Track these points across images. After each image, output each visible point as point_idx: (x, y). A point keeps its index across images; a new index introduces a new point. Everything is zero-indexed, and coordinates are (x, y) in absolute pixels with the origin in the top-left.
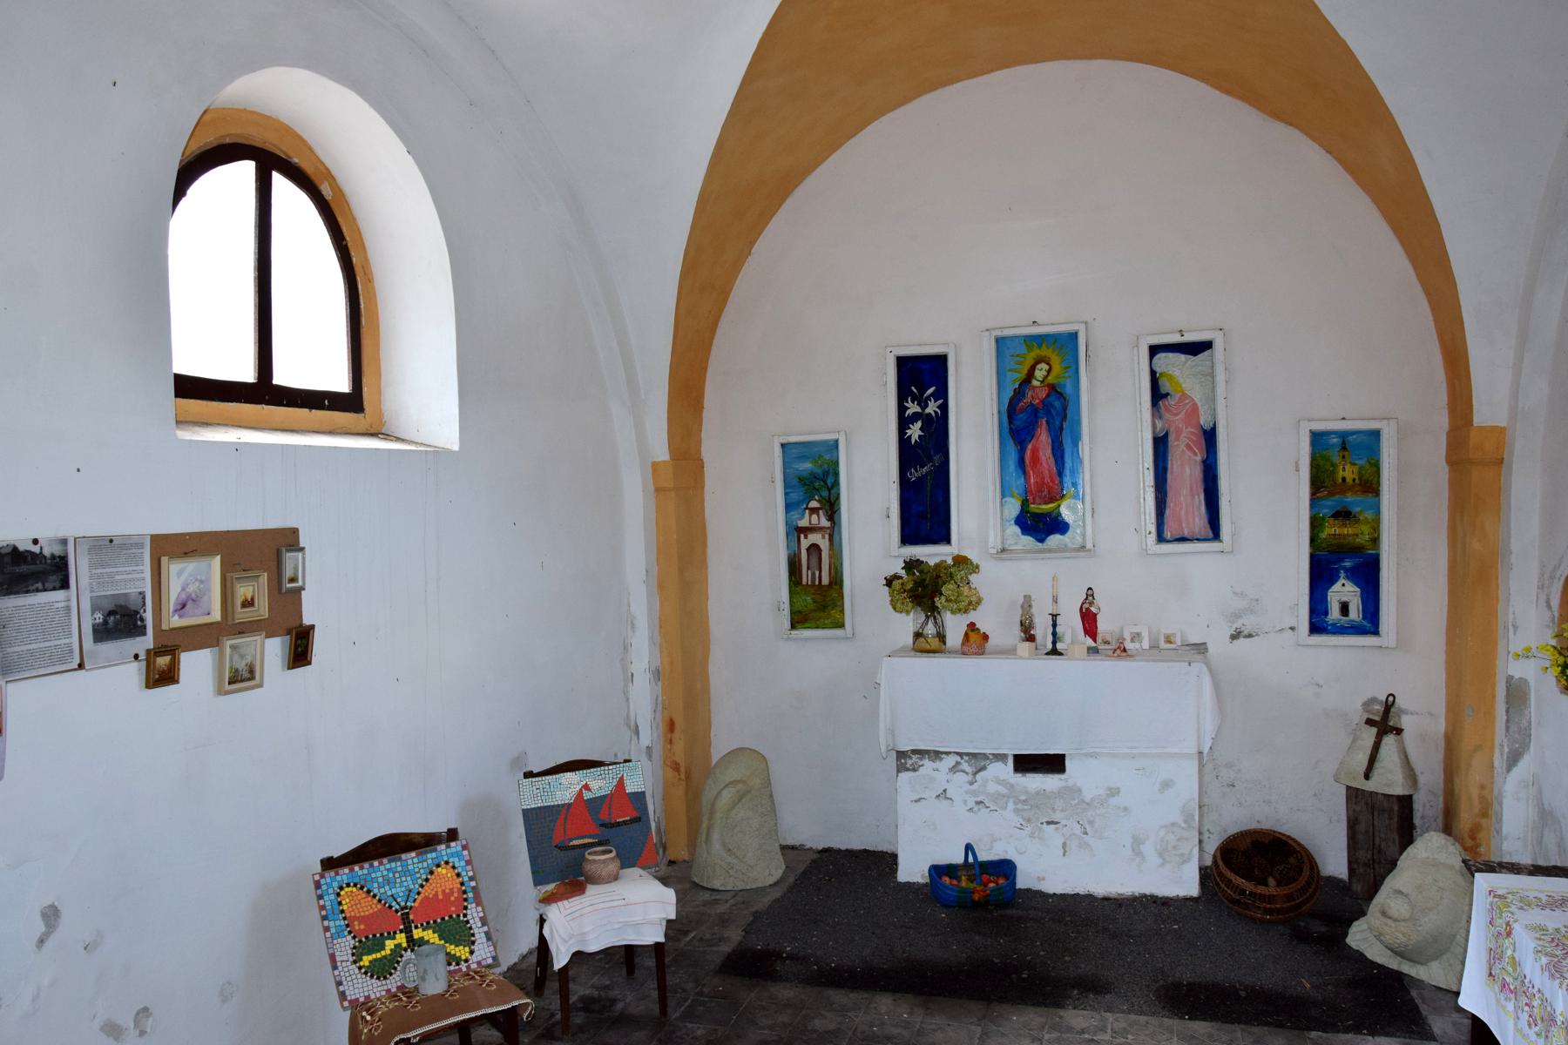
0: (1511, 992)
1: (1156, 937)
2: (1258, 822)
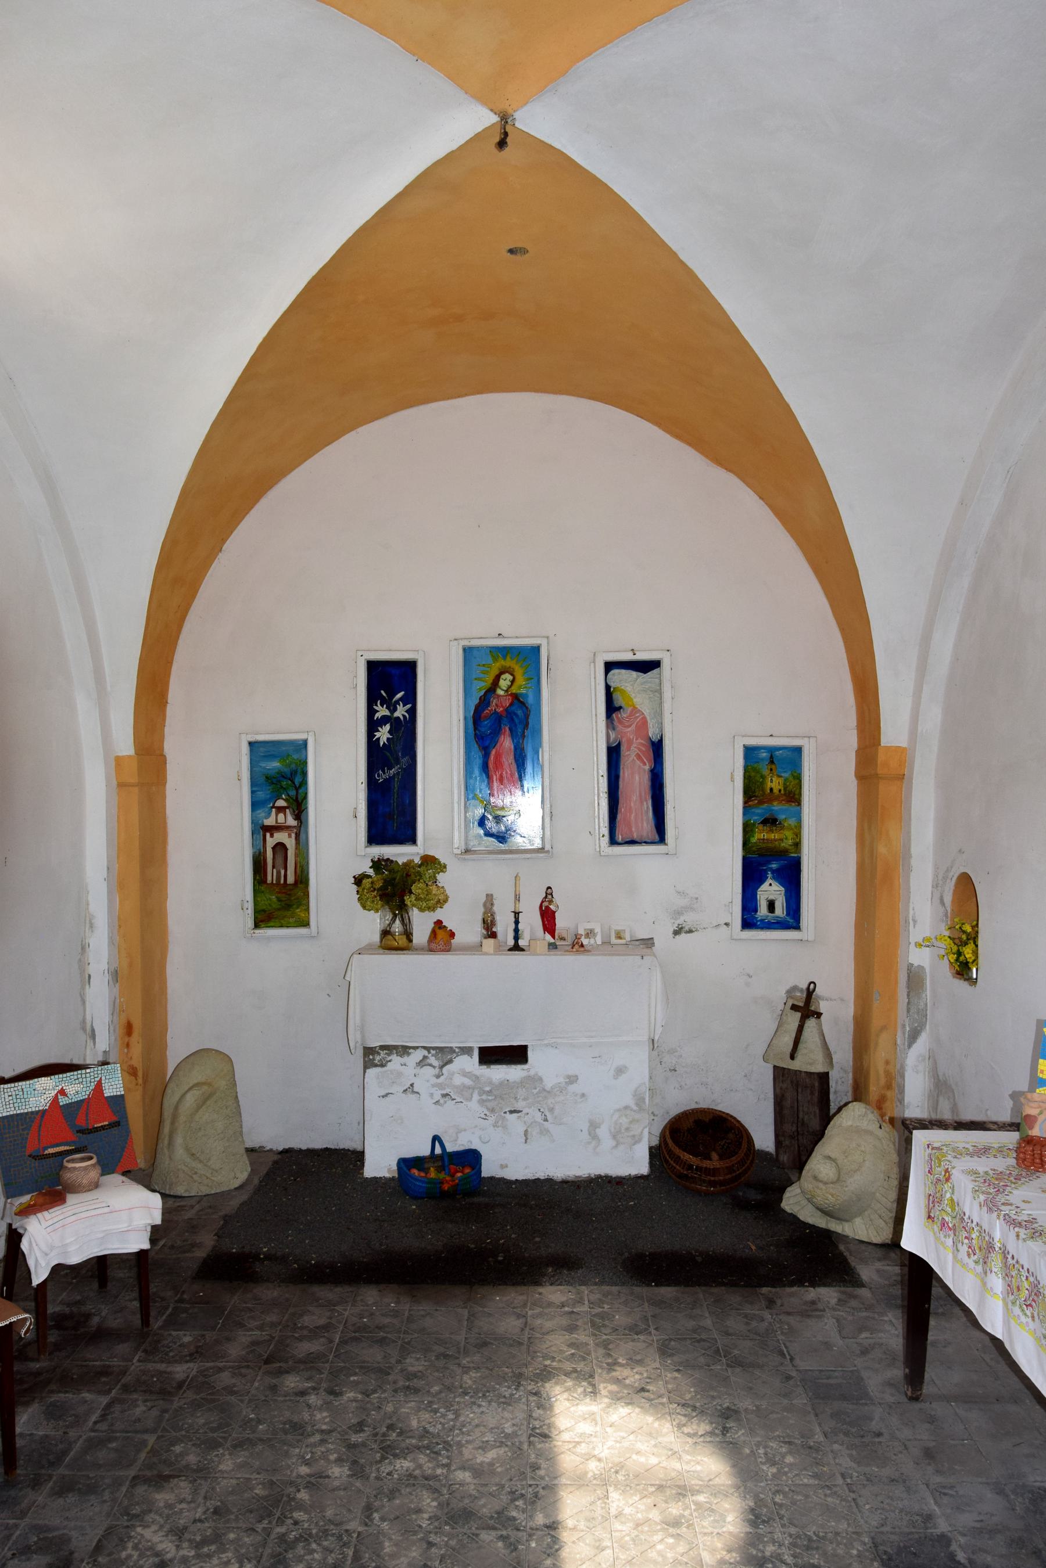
0: (950, 1229)
1: (615, 1214)
2: (696, 1102)
